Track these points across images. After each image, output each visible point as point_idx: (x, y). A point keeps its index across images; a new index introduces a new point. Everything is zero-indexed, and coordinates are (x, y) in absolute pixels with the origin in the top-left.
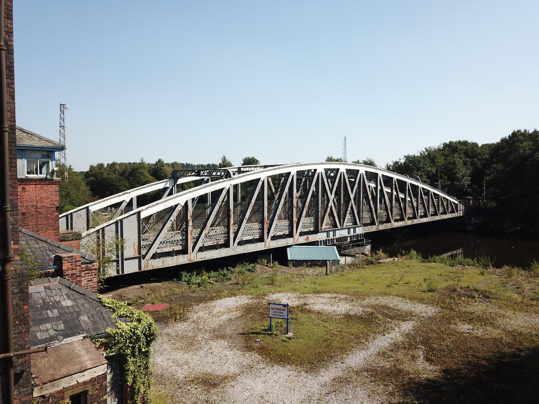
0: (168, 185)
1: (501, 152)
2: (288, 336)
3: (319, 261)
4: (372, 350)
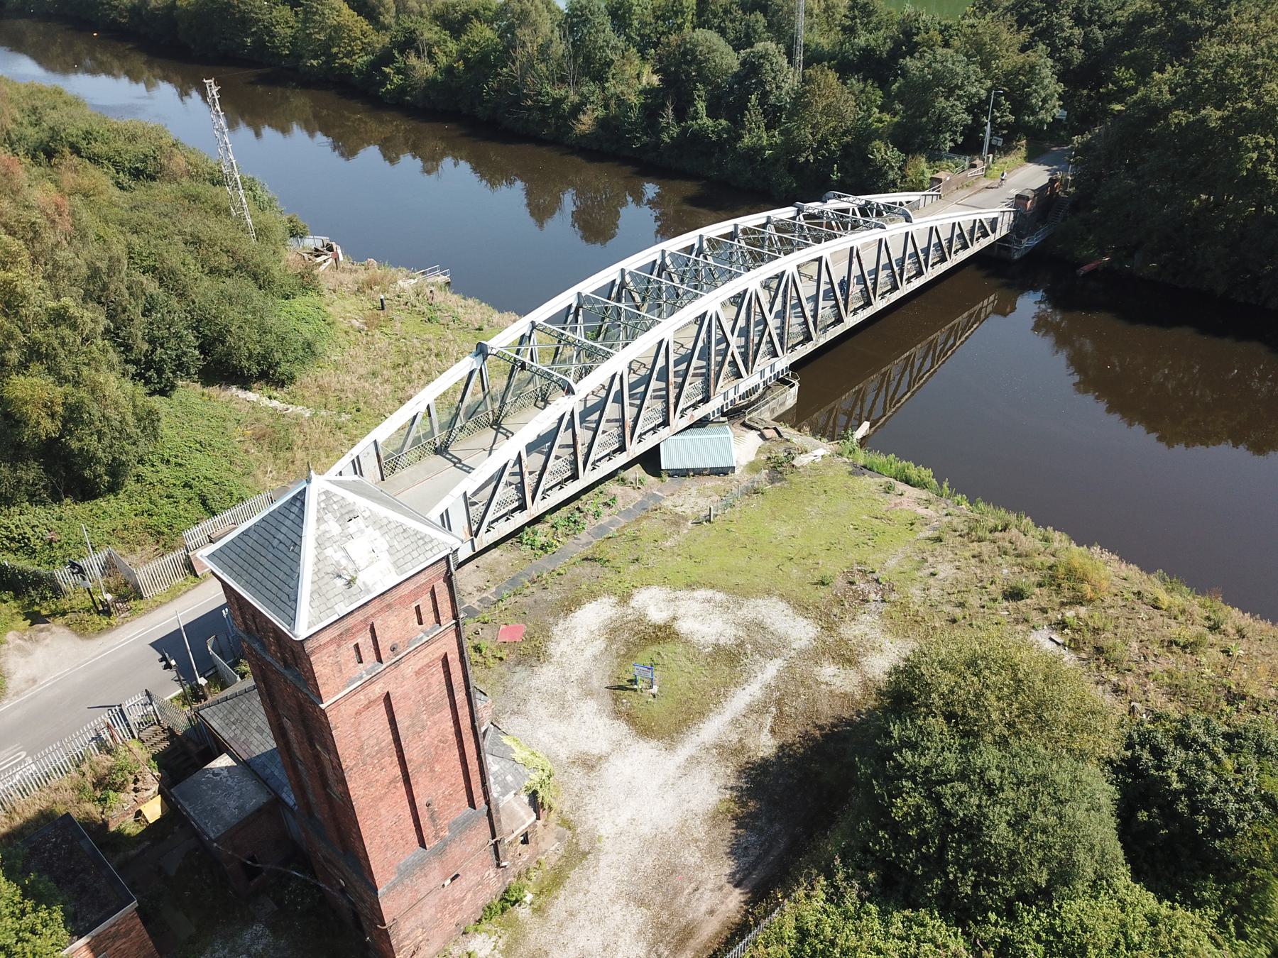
0: (474, 366)
1: (1148, 30)
2: (652, 691)
3: (705, 469)
4: (728, 713)
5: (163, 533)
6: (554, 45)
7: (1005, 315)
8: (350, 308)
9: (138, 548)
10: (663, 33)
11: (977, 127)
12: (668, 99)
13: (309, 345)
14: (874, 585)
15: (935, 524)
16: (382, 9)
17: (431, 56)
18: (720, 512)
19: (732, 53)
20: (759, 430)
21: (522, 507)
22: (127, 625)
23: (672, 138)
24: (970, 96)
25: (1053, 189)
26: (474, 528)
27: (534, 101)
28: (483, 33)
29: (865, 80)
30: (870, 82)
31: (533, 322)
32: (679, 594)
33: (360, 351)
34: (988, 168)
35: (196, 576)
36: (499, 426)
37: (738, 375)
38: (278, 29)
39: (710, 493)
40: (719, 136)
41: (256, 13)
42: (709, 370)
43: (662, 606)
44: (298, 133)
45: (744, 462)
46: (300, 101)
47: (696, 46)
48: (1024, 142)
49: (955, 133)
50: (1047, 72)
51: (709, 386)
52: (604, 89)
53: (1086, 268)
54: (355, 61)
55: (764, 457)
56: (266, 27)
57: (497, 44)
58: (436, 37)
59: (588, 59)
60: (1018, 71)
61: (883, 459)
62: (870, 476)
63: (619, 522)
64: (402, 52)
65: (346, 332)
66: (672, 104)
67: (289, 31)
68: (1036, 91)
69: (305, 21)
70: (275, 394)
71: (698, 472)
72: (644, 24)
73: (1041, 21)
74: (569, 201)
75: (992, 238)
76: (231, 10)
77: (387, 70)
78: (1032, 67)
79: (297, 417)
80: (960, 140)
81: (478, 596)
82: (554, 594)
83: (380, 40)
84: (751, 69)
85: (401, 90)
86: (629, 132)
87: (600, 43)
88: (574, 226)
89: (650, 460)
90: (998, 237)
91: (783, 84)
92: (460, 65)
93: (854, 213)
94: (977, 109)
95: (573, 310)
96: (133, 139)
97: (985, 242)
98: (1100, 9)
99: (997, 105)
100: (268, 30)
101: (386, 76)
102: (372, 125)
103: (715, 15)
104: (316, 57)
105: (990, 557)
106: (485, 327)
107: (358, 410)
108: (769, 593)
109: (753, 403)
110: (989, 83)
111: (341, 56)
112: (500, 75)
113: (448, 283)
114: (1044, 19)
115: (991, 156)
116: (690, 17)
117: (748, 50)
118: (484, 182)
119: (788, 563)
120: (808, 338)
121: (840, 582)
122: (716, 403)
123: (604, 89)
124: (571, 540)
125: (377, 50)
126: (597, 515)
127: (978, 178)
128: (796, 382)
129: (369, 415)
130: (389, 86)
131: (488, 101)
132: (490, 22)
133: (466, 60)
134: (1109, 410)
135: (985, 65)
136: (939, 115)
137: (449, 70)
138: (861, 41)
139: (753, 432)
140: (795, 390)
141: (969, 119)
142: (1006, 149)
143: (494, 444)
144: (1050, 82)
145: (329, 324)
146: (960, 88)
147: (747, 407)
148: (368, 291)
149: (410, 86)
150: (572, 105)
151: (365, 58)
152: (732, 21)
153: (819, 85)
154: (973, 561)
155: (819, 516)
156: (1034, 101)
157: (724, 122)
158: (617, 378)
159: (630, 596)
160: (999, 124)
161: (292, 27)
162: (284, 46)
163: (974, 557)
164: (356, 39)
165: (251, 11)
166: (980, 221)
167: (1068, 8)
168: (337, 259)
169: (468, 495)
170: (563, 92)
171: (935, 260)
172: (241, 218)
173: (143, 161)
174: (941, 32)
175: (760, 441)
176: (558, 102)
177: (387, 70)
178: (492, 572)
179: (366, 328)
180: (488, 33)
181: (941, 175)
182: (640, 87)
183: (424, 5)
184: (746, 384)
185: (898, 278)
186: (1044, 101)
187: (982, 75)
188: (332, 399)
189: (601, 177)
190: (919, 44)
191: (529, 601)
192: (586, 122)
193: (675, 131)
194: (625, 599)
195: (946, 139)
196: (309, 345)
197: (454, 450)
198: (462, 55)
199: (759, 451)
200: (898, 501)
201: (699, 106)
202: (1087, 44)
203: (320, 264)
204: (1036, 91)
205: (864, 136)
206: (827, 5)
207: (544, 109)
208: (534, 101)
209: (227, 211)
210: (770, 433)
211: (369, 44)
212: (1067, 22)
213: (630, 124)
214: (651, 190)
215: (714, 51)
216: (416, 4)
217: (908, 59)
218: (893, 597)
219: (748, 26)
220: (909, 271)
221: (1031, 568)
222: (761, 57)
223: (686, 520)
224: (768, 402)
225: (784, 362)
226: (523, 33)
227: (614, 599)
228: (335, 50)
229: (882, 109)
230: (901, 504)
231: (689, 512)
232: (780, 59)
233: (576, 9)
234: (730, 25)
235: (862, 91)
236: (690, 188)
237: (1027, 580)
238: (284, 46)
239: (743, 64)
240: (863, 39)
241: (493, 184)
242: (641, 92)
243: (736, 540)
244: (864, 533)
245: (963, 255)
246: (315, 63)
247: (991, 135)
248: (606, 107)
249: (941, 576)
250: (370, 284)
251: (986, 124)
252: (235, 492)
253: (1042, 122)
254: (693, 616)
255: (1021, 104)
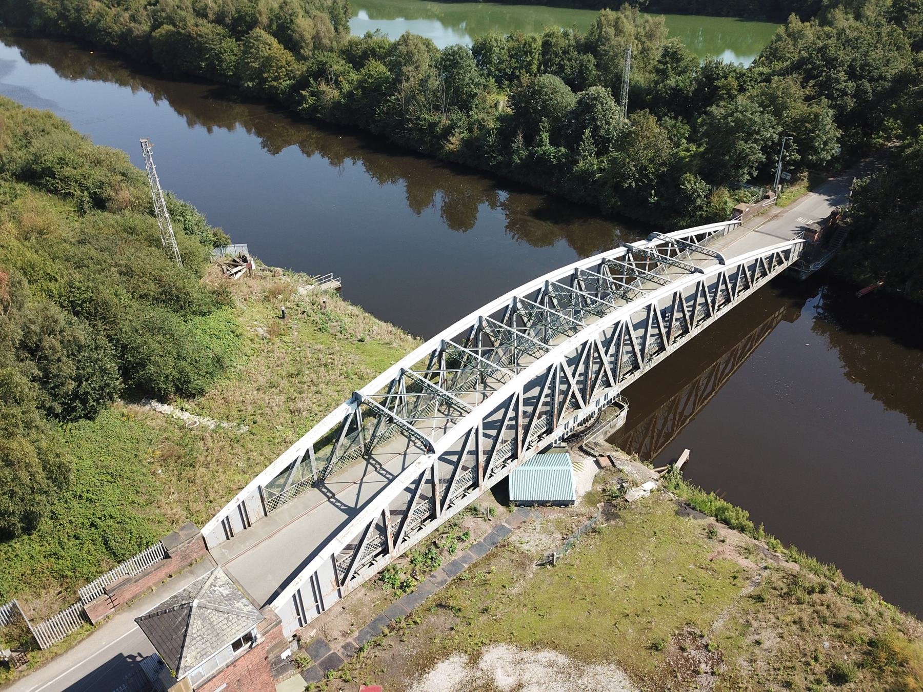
0: (350, 412)
5: (66, 577)
6: (431, 79)
7: (792, 321)
8: (257, 317)
9: (44, 592)
10: (516, 68)
11: (770, 163)
12: (519, 128)
13: (219, 361)
14: (704, 652)
15: (757, 579)
16: (303, 44)
17: (338, 84)
18: (562, 555)
19: (571, 93)
20: (595, 456)
21: (385, 551)
22: (23, 680)
23: (521, 159)
24: (765, 140)
25: (834, 220)
26: (341, 577)
27: (415, 124)
28: (378, 68)
29: (676, 118)
30: (680, 119)
31: (402, 369)
32: (525, 655)
33: (262, 360)
34: (779, 197)
35: (91, 624)
36: (370, 457)
37: (577, 406)
38: (225, 56)
39: (553, 529)
40: (559, 160)
41: (210, 44)
42: (553, 399)
43: (508, 669)
44: (240, 129)
45: (582, 492)
46: (239, 109)
47: (542, 88)
48: (806, 174)
49: (751, 167)
50: (829, 120)
51: (552, 420)
52: (469, 116)
53: (863, 291)
54: (281, 84)
55: (599, 488)
56: (216, 54)
57: (388, 78)
58: (341, 69)
59: (457, 91)
60: (803, 120)
61: (704, 495)
62: (694, 517)
63: (471, 558)
64: (315, 80)
65: (252, 340)
66: (522, 132)
67: (233, 58)
68: (818, 136)
69: (245, 52)
70: (187, 406)
71: (542, 504)
72: (501, 61)
73: (821, 76)
74: (439, 198)
75: (786, 265)
76: (191, 41)
77: (304, 93)
78: (817, 116)
79: (205, 428)
80: (755, 174)
81: (342, 641)
82: (408, 649)
83: (300, 68)
84: (586, 107)
85: (314, 109)
86: (487, 152)
87: (467, 79)
88: (442, 217)
89: (501, 491)
90: (790, 263)
91: (611, 120)
92: (359, 92)
93: (673, 246)
94: (770, 149)
95: (437, 354)
96: (98, 163)
97: (779, 269)
98: (871, 66)
99: (787, 146)
100: (218, 56)
101: (303, 97)
102: (292, 131)
103: (556, 55)
104: (251, 80)
105: (810, 626)
106: (367, 338)
107: (255, 422)
108: (607, 658)
109: (590, 428)
110: (780, 129)
111: (270, 79)
112: (389, 101)
113: (338, 289)
114: (824, 74)
115: (780, 186)
116: (537, 56)
117: (584, 92)
118: (375, 179)
119: (624, 621)
120: (636, 367)
121: (671, 647)
122: (559, 432)
123: (469, 116)
124: (427, 577)
125: (297, 76)
126: (451, 551)
127: (770, 206)
128: (626, 406)
129: (264, 428)
130: (305, 105)
131: (379, 121)
132: (381, 58)
133: (364, 89)
134: (866, 390)
135: (777, 113)
136: (740, 154)
137: (350, 95)
138: (671, 82)
139: (589, 458)
140: (624, 414)
141: (763, 158)
142: (793, 182)
143: (364, 475)
144: (830, 129)
145: (237, 336)
146: (758, 133)
147: (583, 432)
148: (273, 300)
149: (320, 106)
150: (444, 128)
151: (288, 82)
152: (569, 60)
153: (642, 127)
154: (794, 628)
155: (650, 562)
156: (817, 144)
157: (563, 150)
158: (473, 431)
159: (479, 655)
160: (788, 162)
161: (236, 55)
162: (230, 69)
163: (795, 622)
164: (281, 67)
165: (206, 42)
166: (778, 253)
167: (844, 65)
168: (250, 268)
169: (335, 555)
170: (436, 118)
171: (741, 288)
172: (170, 246)
173: (100, 188)
174: (737, 78)
175: (596, 469)
176: (433, 125)
177: (304, 93)
178: (356, 613)
179: (268, 336)
180: (382, 68)
181: (742, 206)
182: (497, 114)
183: (334, 43)
184: (582, 414)
185: (711, 308)
186: (825, 143)
187: (774, 123)
188: (234, 412)
189: (467, 186)
190: (719, 87)
191: (386, 655)
192: (454, 142)
193: (524, 153)
194: (474, 659)
195: (744, 173)
196: (218, 361)
197: (330, 483)
198: (361, 82)
199: (595, 481)
200: (720, 549)
201: (543, 136)
202: (858, 94)
203: (236, 273)
204: (818, 136)
205: (677, 168)
206: (644, 48)
207: (421, 130)
208: (415, 124)
209: (159, 240)
210: (604, 462)
211: (291, 71)
212: (843, 76)
213: (489, 146)
214: (503, 195)
215: (556, 92)
216: (328, 42)
217: (714, 107)
218: (723, 669)
219: (582, 65)
220: (720, 301)
221: (852, 643)
222: (595, 99)
223: (531, 560)
224: (602, 427)
225: (615, 390)
226: (408, 70)
227: (465, 658)
228: (266, 75)
229: (690, 140)
230: (723, 552)
231: (533, 550)
232: (609, 100)
233: (449, 54)
234: (568, 63)
235: (674, 126)
236: (536, 202)
237: (846, 659)
238: (230, 69)
239: (580, 102)
240: (673, 80)
241: (382, 182)
242: (497, 119)
243: (576, 590)
244: (691, 587)
245: (763, 282)
246: (250, 84)
247: (782, 171)
248: (470, 130)
249: (766, 645)
250: (275, 293)
251: (778, 162)
252: (134, 531)
253: (822, 160)
254: (537, 683)
255: (806, 146)
